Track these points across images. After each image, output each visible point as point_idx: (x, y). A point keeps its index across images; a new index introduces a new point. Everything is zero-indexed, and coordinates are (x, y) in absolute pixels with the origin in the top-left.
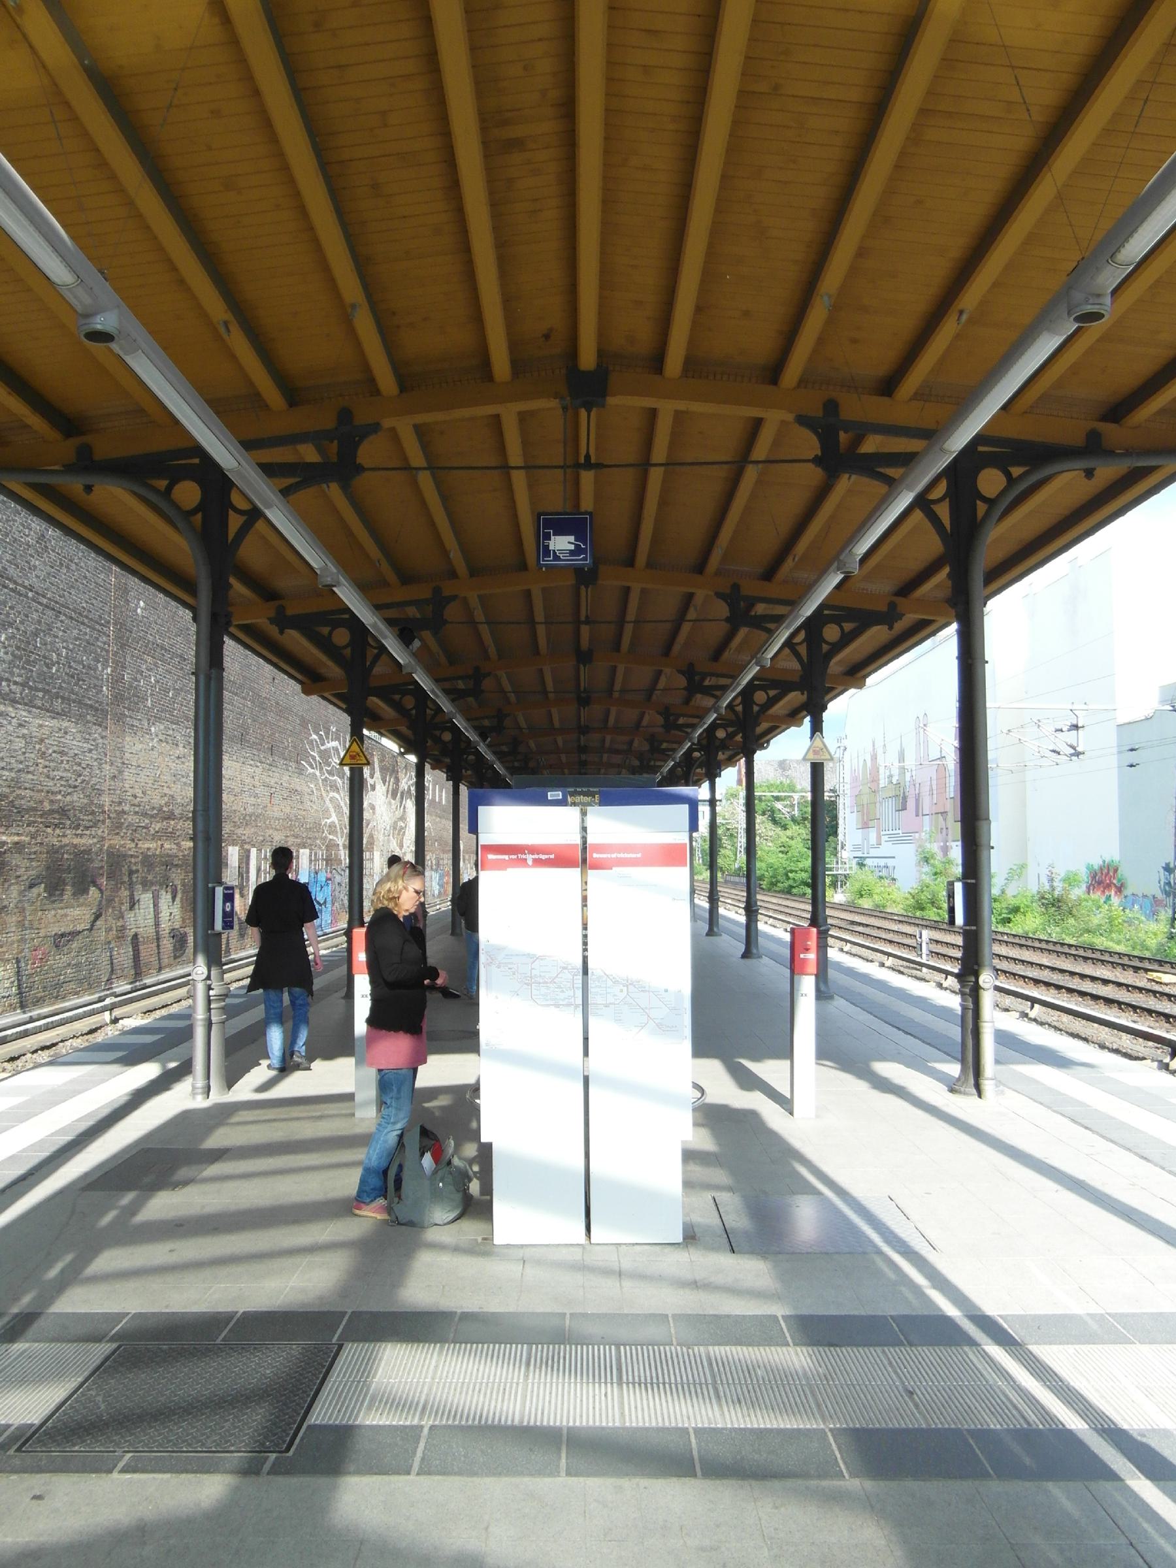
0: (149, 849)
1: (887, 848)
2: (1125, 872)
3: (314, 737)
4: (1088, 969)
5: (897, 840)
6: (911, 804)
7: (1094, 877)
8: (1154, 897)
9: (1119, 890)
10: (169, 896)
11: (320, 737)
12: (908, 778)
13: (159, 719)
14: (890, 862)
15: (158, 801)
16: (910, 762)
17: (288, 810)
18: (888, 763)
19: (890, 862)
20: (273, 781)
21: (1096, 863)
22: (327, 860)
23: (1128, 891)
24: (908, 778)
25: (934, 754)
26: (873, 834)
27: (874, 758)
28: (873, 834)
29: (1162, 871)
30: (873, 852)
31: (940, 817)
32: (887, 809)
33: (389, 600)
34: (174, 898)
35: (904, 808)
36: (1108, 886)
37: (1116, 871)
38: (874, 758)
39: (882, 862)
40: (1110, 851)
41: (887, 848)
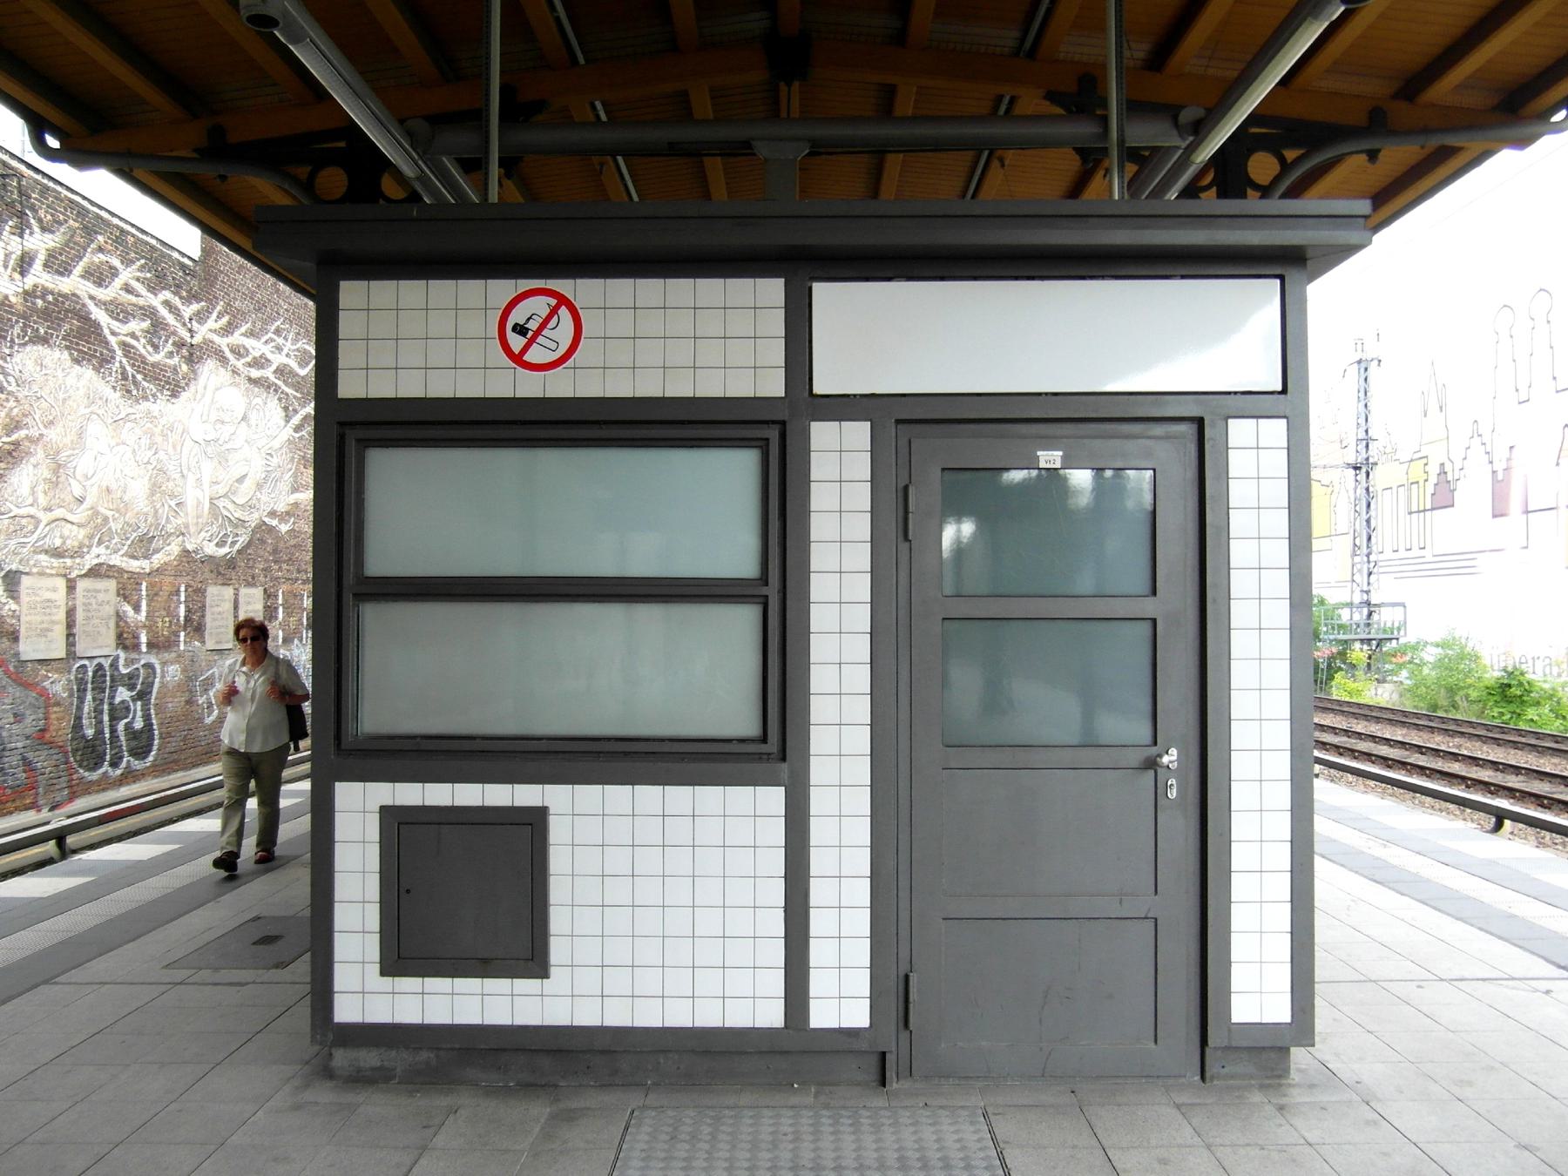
6: (1473, 492)
35: (1444, 497)
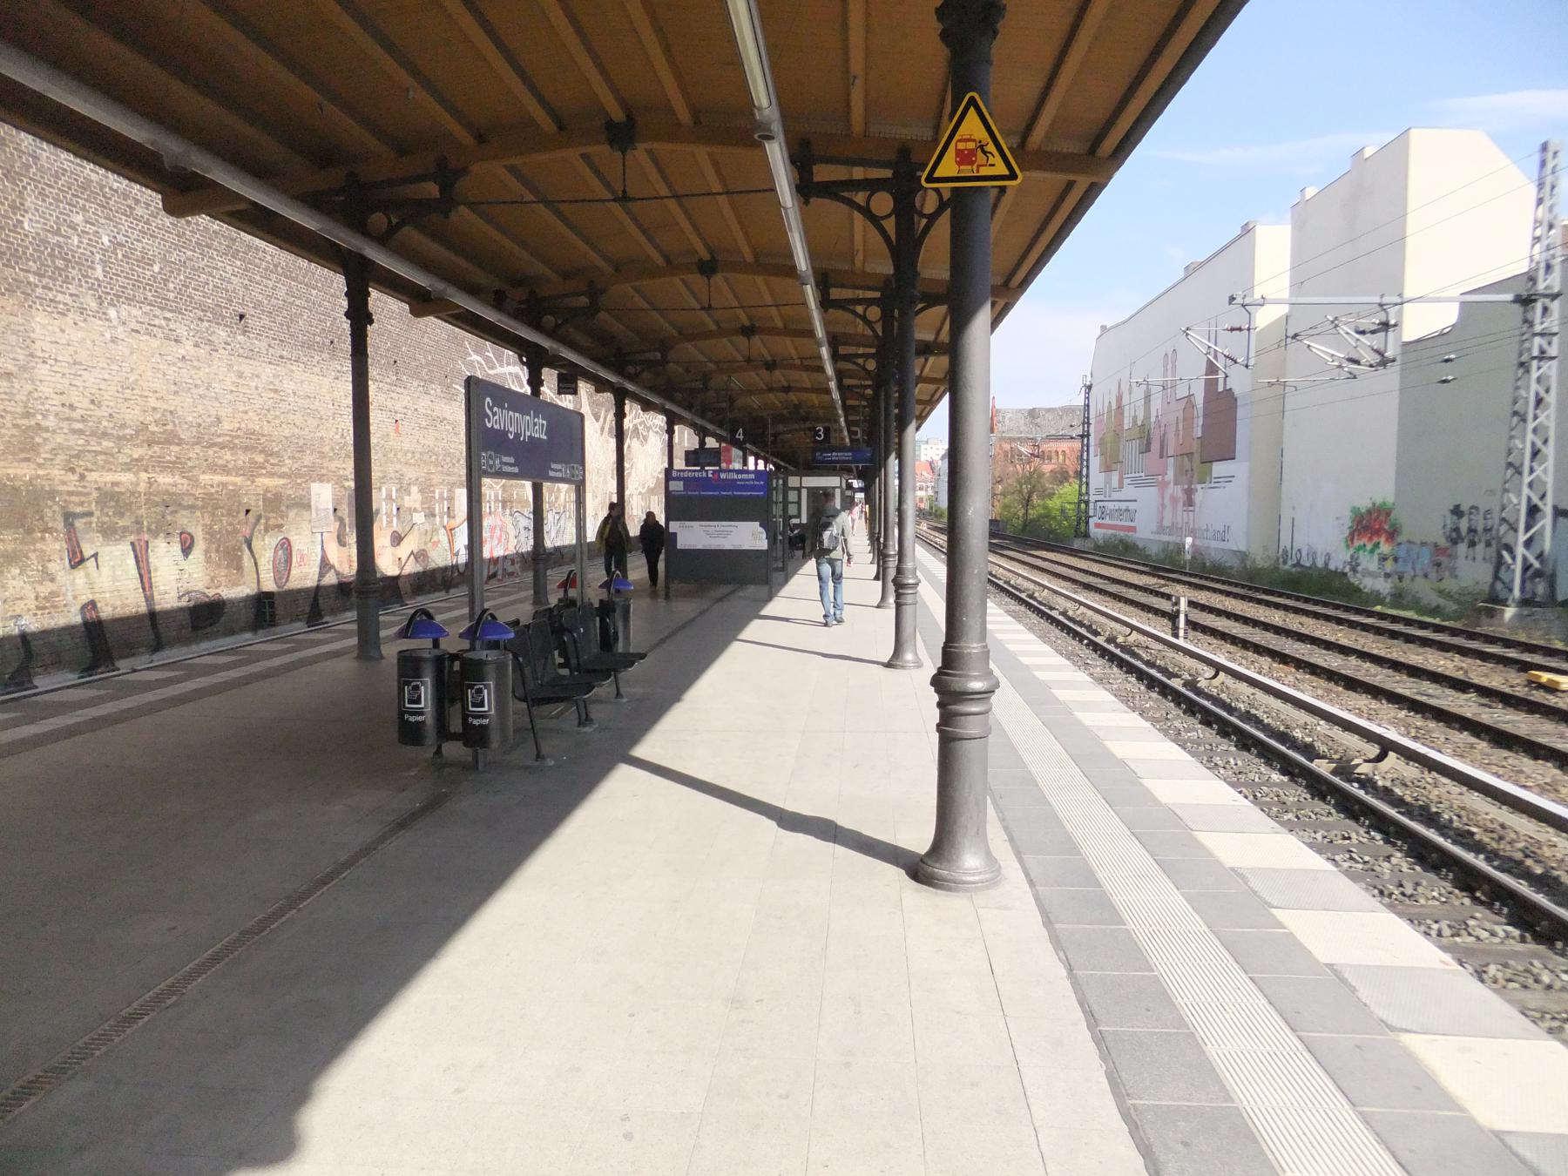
0: (114, 484)
1: (1129, 491)
2: (1400, 516)
3: (475, 357)
4: (1397, 651)
5: (1138, 484)
6: (1155, 447)
7: (1360, 522)
8: (1436, 545)
9: (1392, 535)
10: (176, 548)
11: (487, 359)
12: (1153, 419)
13: (118, 298)
14: (1132, 506)
15: (132, 415)
16: (1156, 403)
17: (430, 442)
18: (1134, 411)
19: (1132, 506)
20: (398, 407)
21: (1364, 504)
22: (504, 503)
23: (1401, 538)
24: (1153, 419)
25: (1182, 392)
26: (1115, 477)
27: (1119, 398)
28: (1115, 477)
29: (1449, 515)
30: (1115, 496)
31: (1186, 459)
32: (1131, 450)
33: (1382, 653)
34: (187, 550)
35: (1148, 450)
36: (1377, 533)
37: (1388, 514)
38: (1119, 398)
39: (1123, 506)
40: (1383, 491)
41: (1129, 491)
